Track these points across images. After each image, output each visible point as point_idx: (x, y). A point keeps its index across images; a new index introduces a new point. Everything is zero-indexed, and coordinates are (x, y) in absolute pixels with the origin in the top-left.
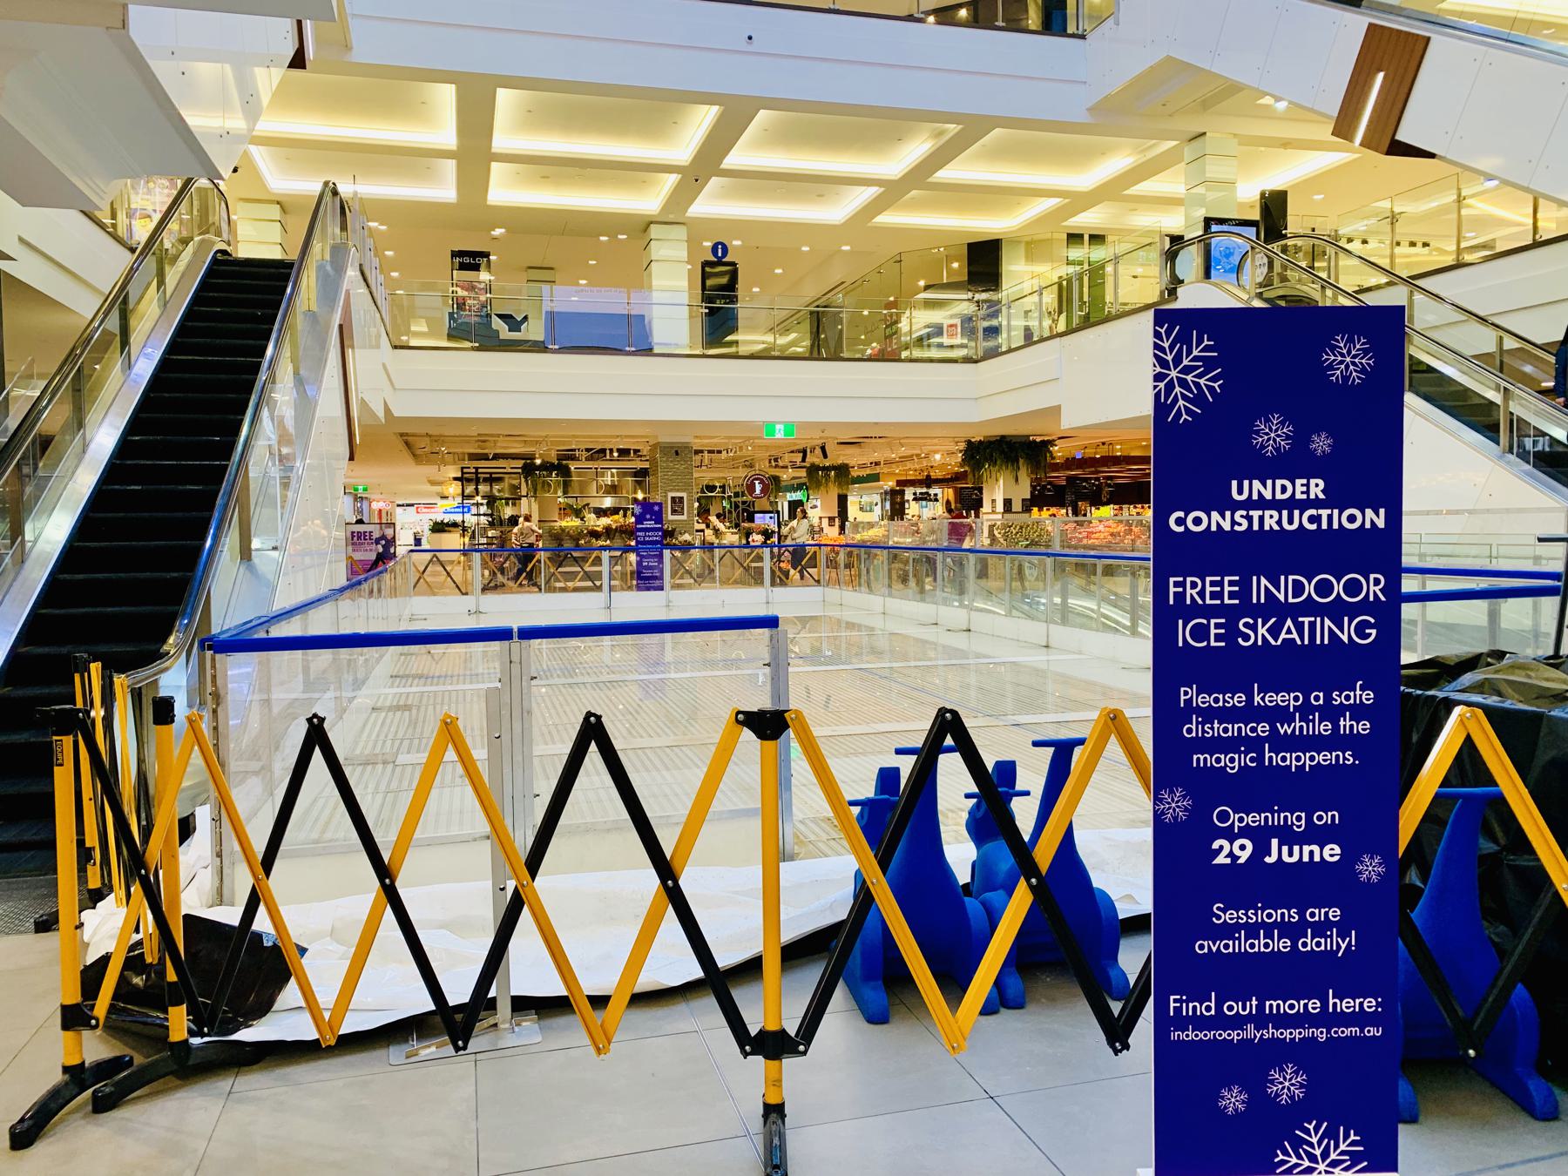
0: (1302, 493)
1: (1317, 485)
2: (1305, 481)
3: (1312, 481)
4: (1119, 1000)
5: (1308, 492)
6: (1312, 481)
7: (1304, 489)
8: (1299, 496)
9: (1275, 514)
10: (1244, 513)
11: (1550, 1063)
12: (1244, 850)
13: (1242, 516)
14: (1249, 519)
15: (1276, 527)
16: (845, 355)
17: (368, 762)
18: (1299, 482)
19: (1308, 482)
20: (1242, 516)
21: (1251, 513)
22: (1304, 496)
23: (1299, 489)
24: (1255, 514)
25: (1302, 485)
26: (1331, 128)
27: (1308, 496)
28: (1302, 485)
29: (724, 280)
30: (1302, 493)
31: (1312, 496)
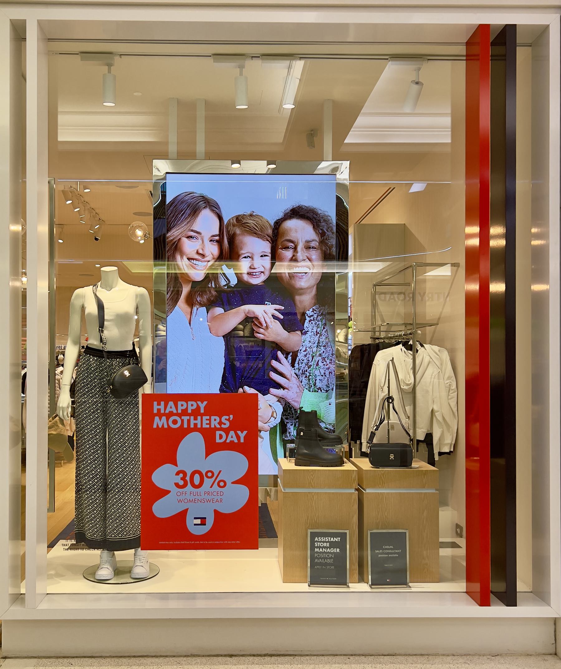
0: (207, 424)
1: (215, 420)
2: (208, 417)
3: (212, 417)
4: (348, 161)
5: (210, 424)
6: (212, 417)
7: (208, 422)
8: (335, 551)
9: (326, 543)
10: (317, 543)
11: (388, 580)
12: (332, 567)
13: (226, 419)
14: (318, 544)
15: (326, 546)
16: (324, 160)
17: (255, 172)
18: (335, 549)
19: (210, 418)
20: (226, 419)
21: (318, 543)
22: (208, 426)
23: (335, 550)
24: (319, 543)
25: (207, 420)
26: (294, 464)
27: (210, 426)
28: (207, 420)
29: (319, 384)
30: (207, 424)
31: (213, 426)
